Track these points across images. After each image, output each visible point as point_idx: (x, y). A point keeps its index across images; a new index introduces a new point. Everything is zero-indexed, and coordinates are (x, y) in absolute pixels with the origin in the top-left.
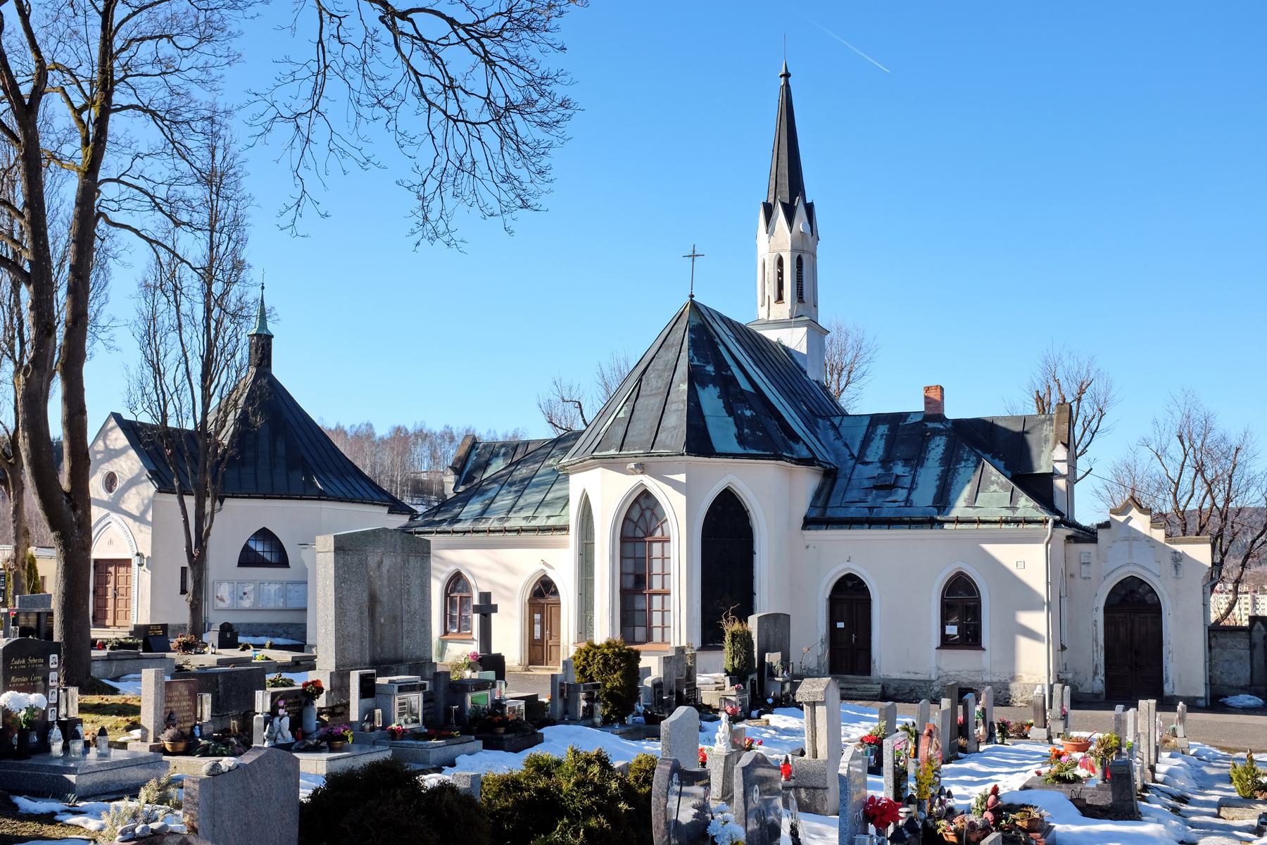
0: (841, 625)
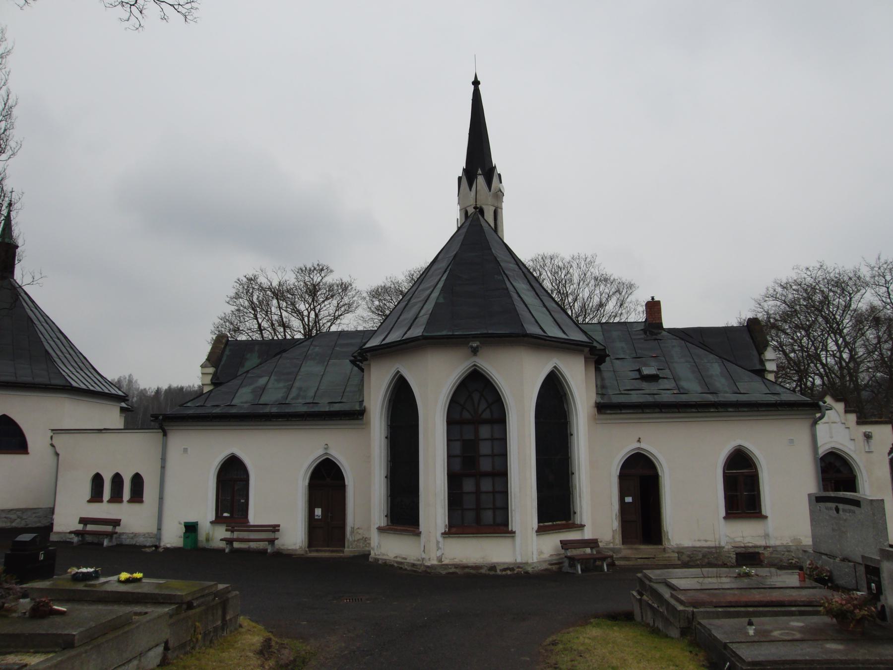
0: (629, 499)
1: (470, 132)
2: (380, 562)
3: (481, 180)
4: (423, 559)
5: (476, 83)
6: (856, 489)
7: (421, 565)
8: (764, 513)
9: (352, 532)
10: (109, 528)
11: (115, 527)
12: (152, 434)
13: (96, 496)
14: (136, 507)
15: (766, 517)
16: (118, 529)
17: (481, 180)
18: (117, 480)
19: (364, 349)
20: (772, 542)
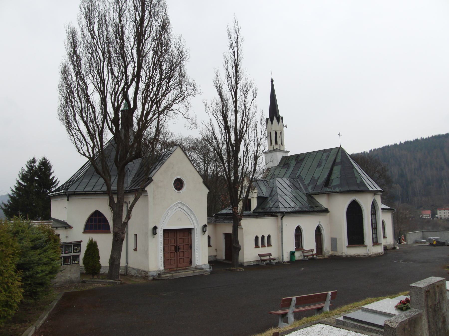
1: (428, 139)
2: (349, 256)
3: (275, 120)
4: (368, 253)
5: (272, 81)
6: (226, 238)
7: (367, 255)
8: (386, 236)
9: (326, 249)
10: (268, 258)
11: (270, 256)
12: (271, 219)
13: (257, 246)
14: (270, 248)
15: (386, 238)
16: (271, 257)
17: (275, 120)
18: (263, 237)
19: (382, 189)
20: (388, 244)
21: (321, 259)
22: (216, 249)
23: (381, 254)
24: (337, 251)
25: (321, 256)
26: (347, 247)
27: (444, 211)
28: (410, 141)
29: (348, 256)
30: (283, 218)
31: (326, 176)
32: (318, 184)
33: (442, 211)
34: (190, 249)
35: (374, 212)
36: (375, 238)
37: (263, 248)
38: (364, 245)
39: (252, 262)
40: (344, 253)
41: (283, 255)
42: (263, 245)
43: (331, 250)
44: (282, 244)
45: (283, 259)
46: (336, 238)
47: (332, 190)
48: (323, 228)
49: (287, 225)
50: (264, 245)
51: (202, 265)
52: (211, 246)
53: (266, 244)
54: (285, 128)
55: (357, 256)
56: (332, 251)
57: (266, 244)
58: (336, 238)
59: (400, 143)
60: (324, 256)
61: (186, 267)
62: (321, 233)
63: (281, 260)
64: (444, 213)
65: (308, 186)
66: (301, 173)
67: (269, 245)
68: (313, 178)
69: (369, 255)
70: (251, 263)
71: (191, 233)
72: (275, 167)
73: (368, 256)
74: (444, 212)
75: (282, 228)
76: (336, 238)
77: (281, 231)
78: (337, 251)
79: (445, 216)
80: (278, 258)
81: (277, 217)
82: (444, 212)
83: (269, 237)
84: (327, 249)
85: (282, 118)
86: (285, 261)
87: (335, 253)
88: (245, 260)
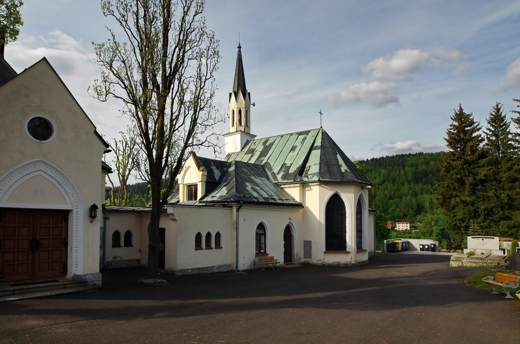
2: (326, 265)
5: (240, 47)
7: (350, 264)
9: (297, 255)
13: (198, 246)
14: (218, 251)
18: (209, 235)
21: (290, 268)
22: (140, 251)
23: (366, 262)
24: (311, 258)
25: (291, 264)
26: (325, 252)
27: (403, 224)
28: (377, 159)
29: (325, 264)
30: (240, 210)
31: (301, 162)
32: (290, 172)
33: (401, 225)
34: (64, 246)
35: (360, 211)
36: (359, 243)
37: (208, 251)
38: (346, 251)
39: (190, 271)
40: (320, 261)
41: (237, 262)
42: (208, 246)
43: (303, 257)
44: (237, 245)
45: (237, 267)
46: (310, 242)
47: (308, 179)
48: (295, 226)
49: (245, 219)
50: (210, 246)
51: (87, 275)
52: (133, 246)
53: (213, 245)
54: (252, 106)
55: (336, 264)
56: (304, 257)
57: (213, 245)
58: (311, 241)
59: (367, 159)
60: (293, 264)
61: (55, 279)
62: (292, 234)
63: (234, 268)
64: (403, 226)
65: (278, 173)
66: (268, 159)
67: (218, 246)
68: (284, 165)
69: (351, 264)
70: (188, 271)
71: (66, 219)
72: (237, 153)
73: (351, 265)
74: (403, 225)
75: (237, 224)
76: (310, 242)
77: (235, 228)
78: (311, 258)
79: (403, 229)
80: (231, 265)
81: (231, 208)
82: (403, 225)
83: (218, 235)
84: (298, 254)
85: (249, 94)
86: (240, 270)
87: (308, 260)
88: (179, 268)
